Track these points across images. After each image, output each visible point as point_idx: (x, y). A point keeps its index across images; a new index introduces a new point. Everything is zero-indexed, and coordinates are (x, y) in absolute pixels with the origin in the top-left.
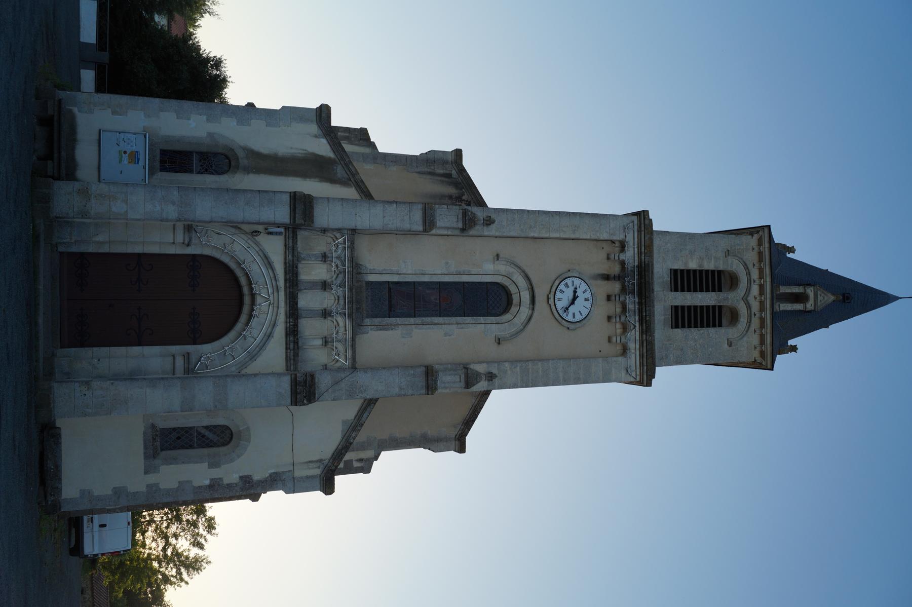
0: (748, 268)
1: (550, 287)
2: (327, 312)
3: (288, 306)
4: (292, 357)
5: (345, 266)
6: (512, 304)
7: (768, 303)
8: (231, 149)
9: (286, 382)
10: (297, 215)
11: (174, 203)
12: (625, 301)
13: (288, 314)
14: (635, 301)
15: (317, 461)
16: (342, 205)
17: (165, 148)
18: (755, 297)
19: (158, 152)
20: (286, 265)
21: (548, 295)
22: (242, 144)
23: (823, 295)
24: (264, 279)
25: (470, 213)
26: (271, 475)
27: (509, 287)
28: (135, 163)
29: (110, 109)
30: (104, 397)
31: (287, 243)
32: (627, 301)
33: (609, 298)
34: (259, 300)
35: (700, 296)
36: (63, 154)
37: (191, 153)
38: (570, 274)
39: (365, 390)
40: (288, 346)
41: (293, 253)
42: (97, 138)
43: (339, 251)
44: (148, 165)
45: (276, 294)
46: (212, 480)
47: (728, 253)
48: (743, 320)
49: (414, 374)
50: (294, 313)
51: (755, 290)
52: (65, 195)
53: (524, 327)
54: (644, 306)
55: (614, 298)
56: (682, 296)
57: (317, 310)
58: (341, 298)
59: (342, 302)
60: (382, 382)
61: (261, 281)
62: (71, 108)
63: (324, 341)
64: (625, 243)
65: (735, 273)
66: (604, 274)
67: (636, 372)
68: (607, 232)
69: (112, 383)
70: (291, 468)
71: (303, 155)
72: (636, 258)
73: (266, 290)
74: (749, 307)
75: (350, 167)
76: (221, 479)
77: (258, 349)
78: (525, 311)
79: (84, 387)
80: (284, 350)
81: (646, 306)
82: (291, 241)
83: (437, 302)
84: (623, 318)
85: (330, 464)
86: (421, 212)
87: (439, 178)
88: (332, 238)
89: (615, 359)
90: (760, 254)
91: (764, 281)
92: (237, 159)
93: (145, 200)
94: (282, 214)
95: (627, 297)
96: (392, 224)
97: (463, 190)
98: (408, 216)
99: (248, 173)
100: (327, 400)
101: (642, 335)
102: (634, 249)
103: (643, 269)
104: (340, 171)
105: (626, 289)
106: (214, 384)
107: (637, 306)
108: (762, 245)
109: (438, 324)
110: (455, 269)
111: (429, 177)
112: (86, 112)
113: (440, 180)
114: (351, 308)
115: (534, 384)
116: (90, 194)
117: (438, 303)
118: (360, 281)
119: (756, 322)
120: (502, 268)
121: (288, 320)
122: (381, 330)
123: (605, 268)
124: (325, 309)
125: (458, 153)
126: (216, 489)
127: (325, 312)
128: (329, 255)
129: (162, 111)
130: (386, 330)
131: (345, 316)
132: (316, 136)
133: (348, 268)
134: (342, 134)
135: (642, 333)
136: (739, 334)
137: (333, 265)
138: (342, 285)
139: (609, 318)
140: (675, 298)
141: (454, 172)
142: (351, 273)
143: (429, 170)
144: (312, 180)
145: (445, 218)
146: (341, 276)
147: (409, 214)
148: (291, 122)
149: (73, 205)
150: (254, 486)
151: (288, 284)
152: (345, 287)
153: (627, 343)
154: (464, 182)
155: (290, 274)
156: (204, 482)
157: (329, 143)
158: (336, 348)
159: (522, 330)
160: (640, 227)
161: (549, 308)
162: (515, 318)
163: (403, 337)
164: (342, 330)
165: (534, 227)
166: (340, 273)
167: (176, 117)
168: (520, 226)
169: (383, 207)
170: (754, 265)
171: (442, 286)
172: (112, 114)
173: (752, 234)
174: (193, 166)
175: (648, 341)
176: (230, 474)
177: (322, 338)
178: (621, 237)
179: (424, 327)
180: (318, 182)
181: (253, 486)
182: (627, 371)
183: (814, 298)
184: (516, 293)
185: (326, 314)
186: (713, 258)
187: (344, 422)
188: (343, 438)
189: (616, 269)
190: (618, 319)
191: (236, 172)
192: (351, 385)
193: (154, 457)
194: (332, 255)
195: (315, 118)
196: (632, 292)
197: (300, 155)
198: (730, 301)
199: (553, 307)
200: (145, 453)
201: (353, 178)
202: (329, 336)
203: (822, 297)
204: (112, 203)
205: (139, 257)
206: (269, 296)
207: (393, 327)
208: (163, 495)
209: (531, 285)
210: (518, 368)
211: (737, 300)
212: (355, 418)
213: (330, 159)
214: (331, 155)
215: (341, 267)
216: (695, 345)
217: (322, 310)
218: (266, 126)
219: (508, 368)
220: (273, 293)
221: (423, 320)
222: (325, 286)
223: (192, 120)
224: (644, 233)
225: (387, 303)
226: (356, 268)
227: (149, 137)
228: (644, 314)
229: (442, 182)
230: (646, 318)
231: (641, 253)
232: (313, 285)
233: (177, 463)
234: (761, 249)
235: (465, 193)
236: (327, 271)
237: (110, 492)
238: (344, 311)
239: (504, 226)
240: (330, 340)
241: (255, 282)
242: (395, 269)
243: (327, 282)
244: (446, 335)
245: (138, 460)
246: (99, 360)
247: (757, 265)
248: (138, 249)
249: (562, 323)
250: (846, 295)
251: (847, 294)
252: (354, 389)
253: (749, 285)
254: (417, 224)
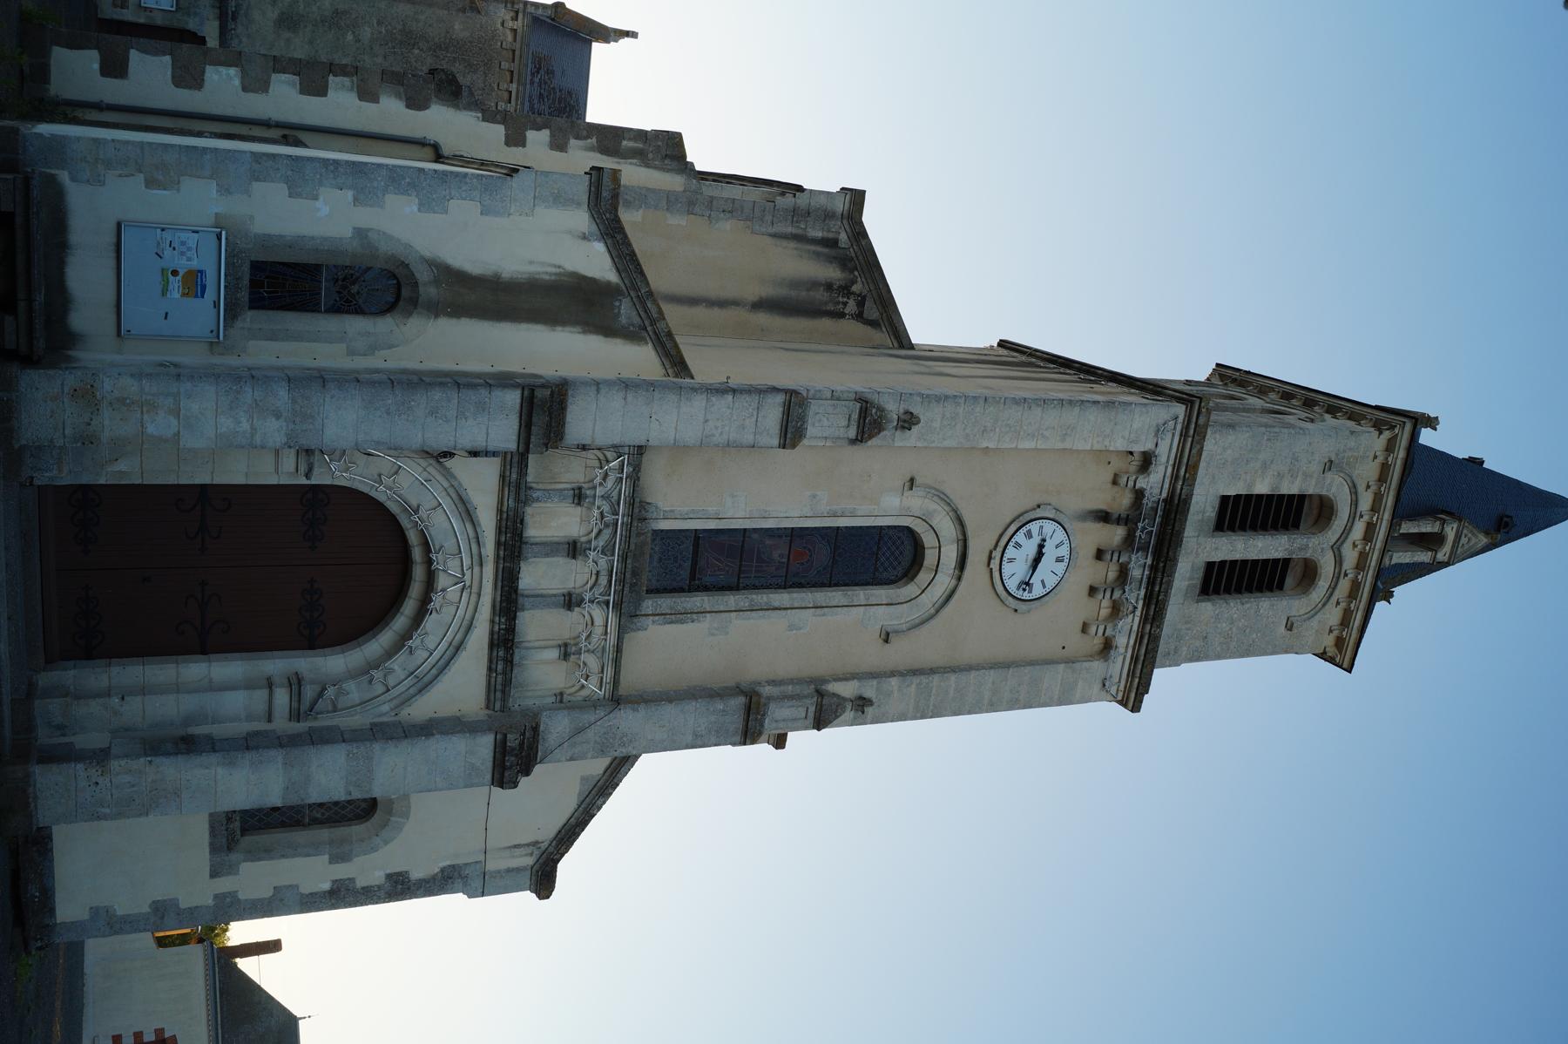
0: (1356, 493)
1: (996, 537)
2: (574, 600)
3: (499, 592)
4: (499, 687)
5: (618, 514)
6: (922, 565)
7: (1375, 557)
8: (403, 262)
9: (484, 746)
10: (533, 439)
11: (278, 416)
12: (1129, 563)
13: (498, 608)
14: (1145, 563)
15: (528, 845)
16: (625, 399)
17: (261, 258)
18: (1354, 543)
19: (246, 268)
20: (501, 515)
21: (991, 552)
22: (427, 254)
23: (1470, 535)
24: (455, 540)
25: (874, 411)
26: (443, 870)
27: (922, 535)
28: (196, 296)
29: (142, 175)
30: (133, 786)
31: (508, 473)
32: (1132, 565)
33: (1099, 555)
34: (442, 581)
35: (1260, 545)
36: (40, 298)
37: (318, 267)
38: (1039, 513)
39: (631, 741)
40: (494, 666)
41: (518, 493)
42: (114, 240)
43: (610, 483)
44: (225, 298)
45: (477, 569)
46: (334, 882)
47: (1329, 465)
48: (1323, 584)
49: (724, 711)
50: (509, 602)
51: (1358, 531)
52: (46, 402)
53: (937, 611)
54: (1160, 574)
55: (1109, 557)
56: (1229, 546)
57: (555, 595)
58: (604, 574)
59: (603, 580)
60: (664, 726)
61: (449, 545)
62: (53, 172)
63: (562, 652)
64: (1153, 459)
65: (1332, 500)
66: (1101, 511)
67: (1118, 686)
68: (1123, 437)
69: (150, 762)
70: (481, 858)
71: (553, 278)
72: (1166, 486)
73: (457, 562)
74: (1339, 560)
75: (649, 305)
76: (352, 880)
77: (434, 671)
78: (944, 581)
79: (94, 770)
80: (485, 671)
81: (1163, 575)
82: (514, 470)
83: (784, 560)
84: (1117, 594)
85: (551, 849)
86: (781, 409)
87: (813, 248)
88: (599, 459)
89: (1086, 664)
90: (1385, 468)
91: (1378, 518)
92: (416, 284)
93: (217, 411)
94: (502, 430)
95: (1134, 557)
96: (721, 433)
97: (856, 273)
98: (754, 419)
99: (437, 316)
100: (559, 761)
101: (1144, 624)
102: (1166, 468)
103: (1174, 508)
104: (626, 311)
105: (1134, 541)
106: (348, 755)
107: (1147, 572)
108: (1393, 453)
109: (780, 609)
110: (828, 508)
111: (792, 244)
112: (88, 181)
113: (814, 252)
114: (620, 593)
115: (936, 713)
116: (98, 397)
117: (783, 563)
118: (643, 534)
119: (1344, 586)
120: (917, 502)
121: (497, 619)
122: (671, 622)
123: (1103, 497)
124: (570, 594)
125: (856, 198)
126: (342, 897)
127: (570, 600)
128: (588, 492)
129: (258, 180)
130: (682, 623)
131: (608, 608)
132: (584, 237)
133: (623, 516)
134: (631, 144)
135: (1145, 620)
136: (1310, 609)
137: (596, 512)
138: (607, 550)
139: (1092, 591)
140: (1217, 549)
141: (843, 237)
142: (629, 527)
143: (794, 231)
144: (568, 329)
145: (825, 419)
146: (607, 533)
147: (755, 413)
148: (534, 206)
149: (64, 423)
150: (412, 888)
151: (502, 553)
152: (613, 555)
153: (1114, 637)
154: (861, 258)
155: (508, 535)
156: (321, 885)
157: (609, 251)
158: (585, 664)
159: (932, 617)
160: (1186, 427)
161: (988, 575)
162: (923, 595)
163: (713, 635)
164: (598, 630)
165: (991, 430)
166: (607, 526)
167: (287, 194)
168: (964, 429)
169: (707, 401)
170: (1368, 487)
171: (796, 536)
172: (146, 187)
173: (1379, 426)
174: (320, 294)
175: (1152, 636)
176: (369, 868)
177: (560, 646)
178: (1149, 446)
179: (754, 614)
180: (579, 333)
181: (409, 889)
182: (1104, 685)
183: (1454, 542)
184: (932, 548)
185: (570, 601)
186: (1300, 474)
187: (584, 779)
188: (579, 806)
189: (1124, 501)
190: (1108, 594)
191: (410, 314)
192: (605, 733)
193: (230, 849)
194: (593, 492)
195: (585, 198)
196: (1144, 548)
197: (547, 277)
198: (1310, 551)
199: (996, 575)
200: (211, 844)
201: (652, 325)
202: (572, 642)
203: (1467, 539)
204: (146, 417)
205: (204, 492)
206: (464, 575)
207: (695, 616)
208: (244, 909)
209: (964, 534)
210: (914, 686)
211: (1323, 549)
212: (605, 772)
213: (608, 284)
214: (612, 276)
215: (609, 518)
216: (1231, 629)
217: (564, 595)
218: (482, 214)
219: (896, 688)
220: (471, 567)
221: (752, 600)
222: (574, 549)
223: (321, 199)
224: (1192, 441)
225: (688, 565)
226: (638, 507)
227: (226, 239)
228: (1157, 589)
229: (818, 254)
230: (1158, 597)
231: (1177, 477)
232: (550, 548)
233: (272, 858)
234: (1390, 459)
235: (859, 279)
236: (582, 521)
237: (146, 909)
238: (606, 598)
239: (935, 429)
240: (574, 649)
241: (437, 548)
242: (712, 509)
243: (579, 544)
244: (791, 627)
245: (202, 857)
246: (123, 698)
247: (1374, 488)
248: (202, 478)
249: (1007, 602)
250: (1505, 519)
251: (1508, 517)
252: (611, 740)
253: (1349, 524)
254: (768, 434)
